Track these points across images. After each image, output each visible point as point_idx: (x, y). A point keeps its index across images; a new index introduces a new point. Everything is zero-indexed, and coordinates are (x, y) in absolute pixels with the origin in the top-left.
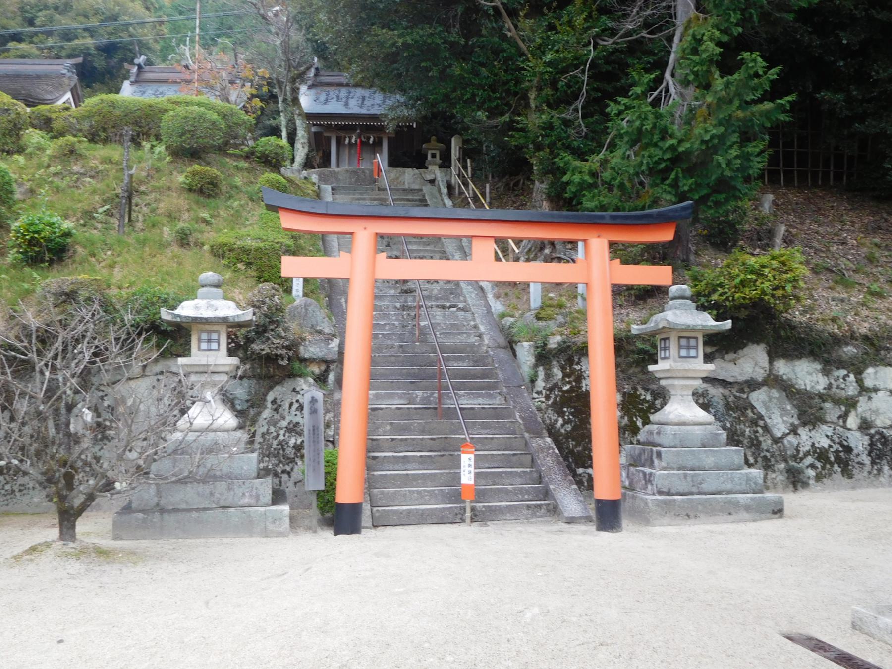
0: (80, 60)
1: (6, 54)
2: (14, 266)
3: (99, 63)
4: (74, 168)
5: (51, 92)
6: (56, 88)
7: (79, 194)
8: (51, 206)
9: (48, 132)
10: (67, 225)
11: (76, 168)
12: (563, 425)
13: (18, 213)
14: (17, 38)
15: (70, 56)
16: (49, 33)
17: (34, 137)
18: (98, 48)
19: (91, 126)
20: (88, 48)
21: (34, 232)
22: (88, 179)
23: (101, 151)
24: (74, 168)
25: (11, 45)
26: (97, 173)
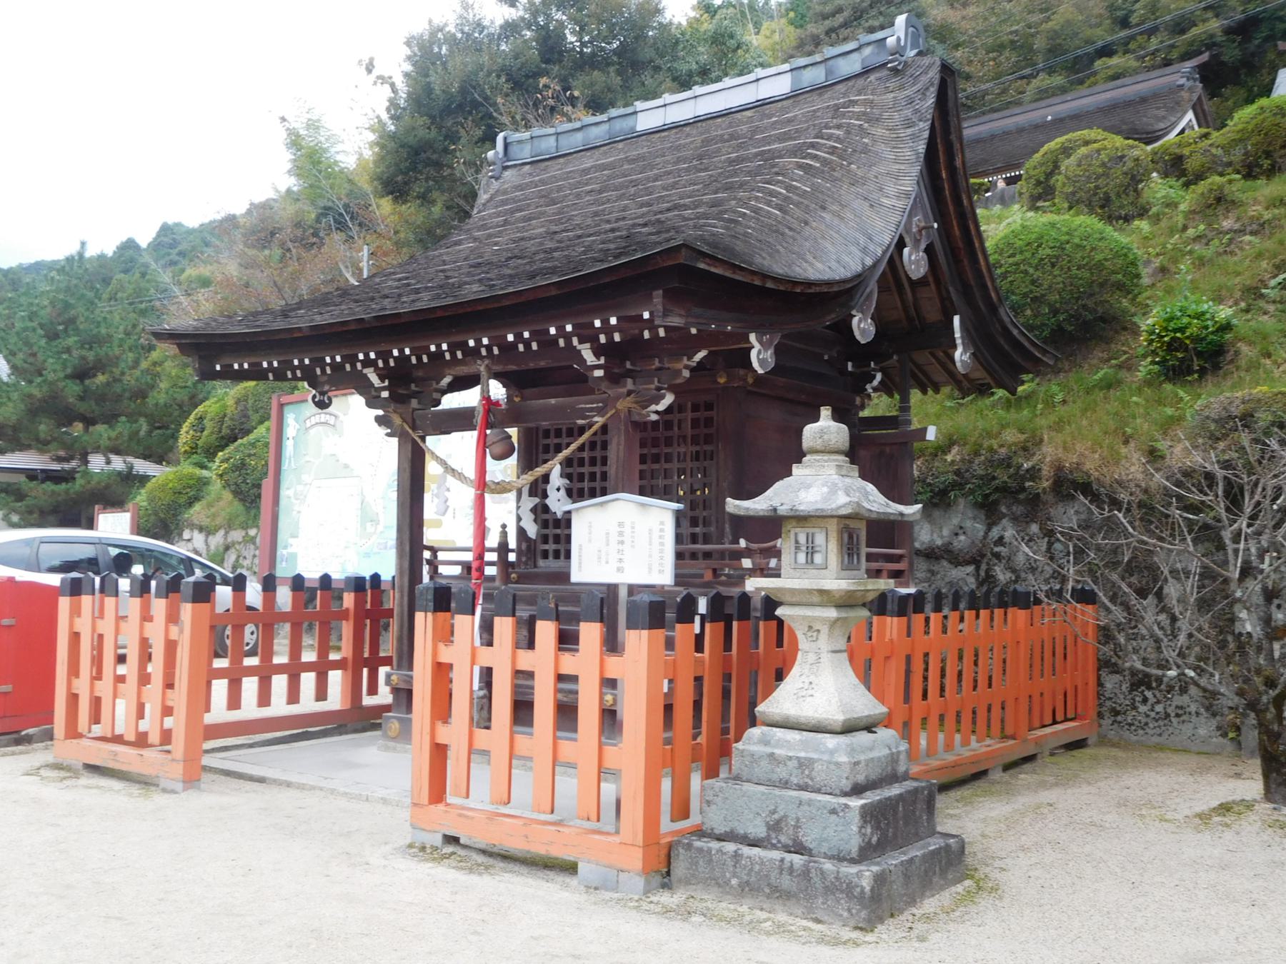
0: (1205, 57)
1: (1092, 79)
2: (1148, 383)
3: (1231, 54)
4: (1225, 224)
5: (1164, 118)
6: (1172, 110)
7: (1235, 263)
8: (1194, 287)
9: (1179, 178)
10: (1224, 313)
11: (1227, 224)
12: (150, 433)
13: (1147, 306)
14: (1107, 51)
15: (1185, 57)
16: (1152, 32)
17: (1158, 188)
18: (1228, 31)
19: (1246, 154)
20: (1212, 36)
21: (1175, 331)
22: (1248, 238)
23: (1267, 189)
24: (1225, 224)
25: (1098, 64)
26: (1262, 225)
